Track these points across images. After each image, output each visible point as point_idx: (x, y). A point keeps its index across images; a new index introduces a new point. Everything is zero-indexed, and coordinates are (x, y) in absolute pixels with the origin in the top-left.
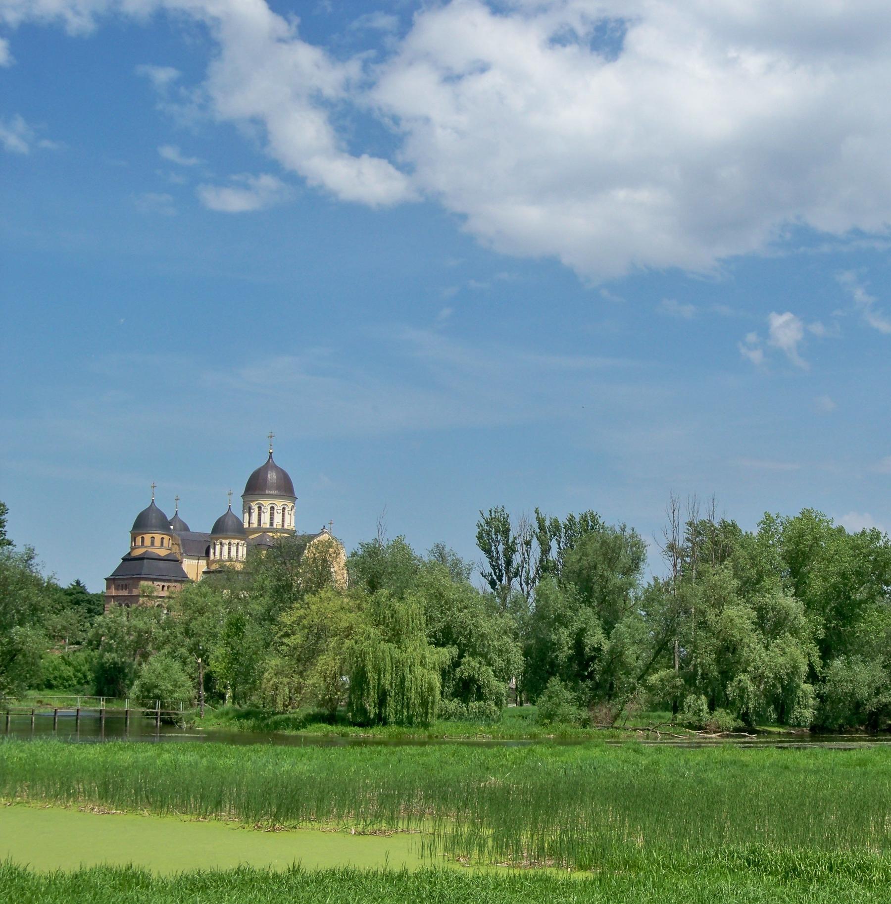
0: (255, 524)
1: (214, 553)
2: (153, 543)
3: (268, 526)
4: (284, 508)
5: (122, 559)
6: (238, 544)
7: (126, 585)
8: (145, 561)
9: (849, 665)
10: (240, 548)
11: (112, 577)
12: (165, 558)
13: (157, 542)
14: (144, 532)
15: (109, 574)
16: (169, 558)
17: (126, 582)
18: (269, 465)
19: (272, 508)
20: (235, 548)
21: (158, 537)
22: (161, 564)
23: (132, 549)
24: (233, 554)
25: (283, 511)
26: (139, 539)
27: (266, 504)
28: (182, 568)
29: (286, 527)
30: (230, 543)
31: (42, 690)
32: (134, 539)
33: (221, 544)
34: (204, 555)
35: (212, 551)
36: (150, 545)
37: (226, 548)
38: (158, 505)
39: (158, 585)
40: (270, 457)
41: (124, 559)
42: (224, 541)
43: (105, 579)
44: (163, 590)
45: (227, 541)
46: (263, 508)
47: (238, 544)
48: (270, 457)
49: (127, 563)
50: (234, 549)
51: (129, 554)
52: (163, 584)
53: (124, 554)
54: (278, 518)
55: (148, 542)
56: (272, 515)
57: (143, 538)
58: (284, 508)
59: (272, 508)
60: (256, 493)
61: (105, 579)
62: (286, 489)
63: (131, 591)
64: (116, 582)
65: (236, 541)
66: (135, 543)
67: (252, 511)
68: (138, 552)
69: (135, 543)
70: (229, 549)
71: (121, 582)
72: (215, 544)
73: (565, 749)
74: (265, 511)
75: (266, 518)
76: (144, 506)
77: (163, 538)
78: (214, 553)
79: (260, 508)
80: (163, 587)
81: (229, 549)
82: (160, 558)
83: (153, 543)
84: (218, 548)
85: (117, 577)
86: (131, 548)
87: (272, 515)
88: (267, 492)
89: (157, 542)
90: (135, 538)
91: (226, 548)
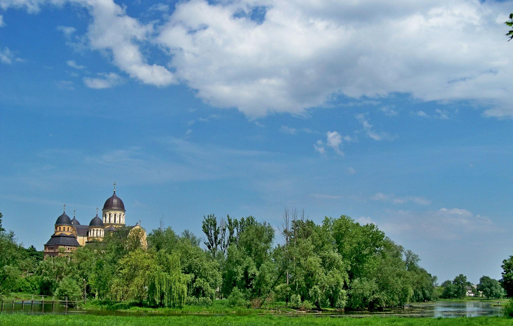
1: (91, 234)
2: (64, 230)
4: (120, 215)
6: (101, 230)
7: (53, 248)
13: (66, 229)
14: (61, 225)
15: (45, 243)
17: (53, 246)
18: (114, 196)
19: (115, 215)
20: (99, 232)
21: (66, 227)
23: (56, 232)
24: (99, 234)
25: (120, 216)
26: (58, 228)
27: (113, 213)
29: (121, 223)
30: (97, 230)
32: (56, 228)
33: (93, 230)
35: (89, 233)
36: (63, 230)
37: (95, 232)
40: (114, 193)
41: (52, 237)
42: (94, 229)
44: (68, 250)
45: (96, 229)
47: (101, 230)
48: (114, 193)
50: (99, 232)
51: (54, 234)
52: (69, 247)
54: (117, 219)
55: (62, 229)
57: (60, 228)
58: (120, 215)
59: (115, 215)
60: (109, 208)
63: (55, 250)
65: (100, 229)
67: (107, 216)
68: (58, 234)
70: (97, 232)
71: (51, 246)
72: (91, 230)
74: (112, 216)
75: (112, 219)
78: (91, 234)
79: (110, 215)
80: (69, 248)
81: (97, 232)
83: (64, 230)
84: (92, 232)
88: (113, 208)
89: (66, 229)
91: (95, 232)
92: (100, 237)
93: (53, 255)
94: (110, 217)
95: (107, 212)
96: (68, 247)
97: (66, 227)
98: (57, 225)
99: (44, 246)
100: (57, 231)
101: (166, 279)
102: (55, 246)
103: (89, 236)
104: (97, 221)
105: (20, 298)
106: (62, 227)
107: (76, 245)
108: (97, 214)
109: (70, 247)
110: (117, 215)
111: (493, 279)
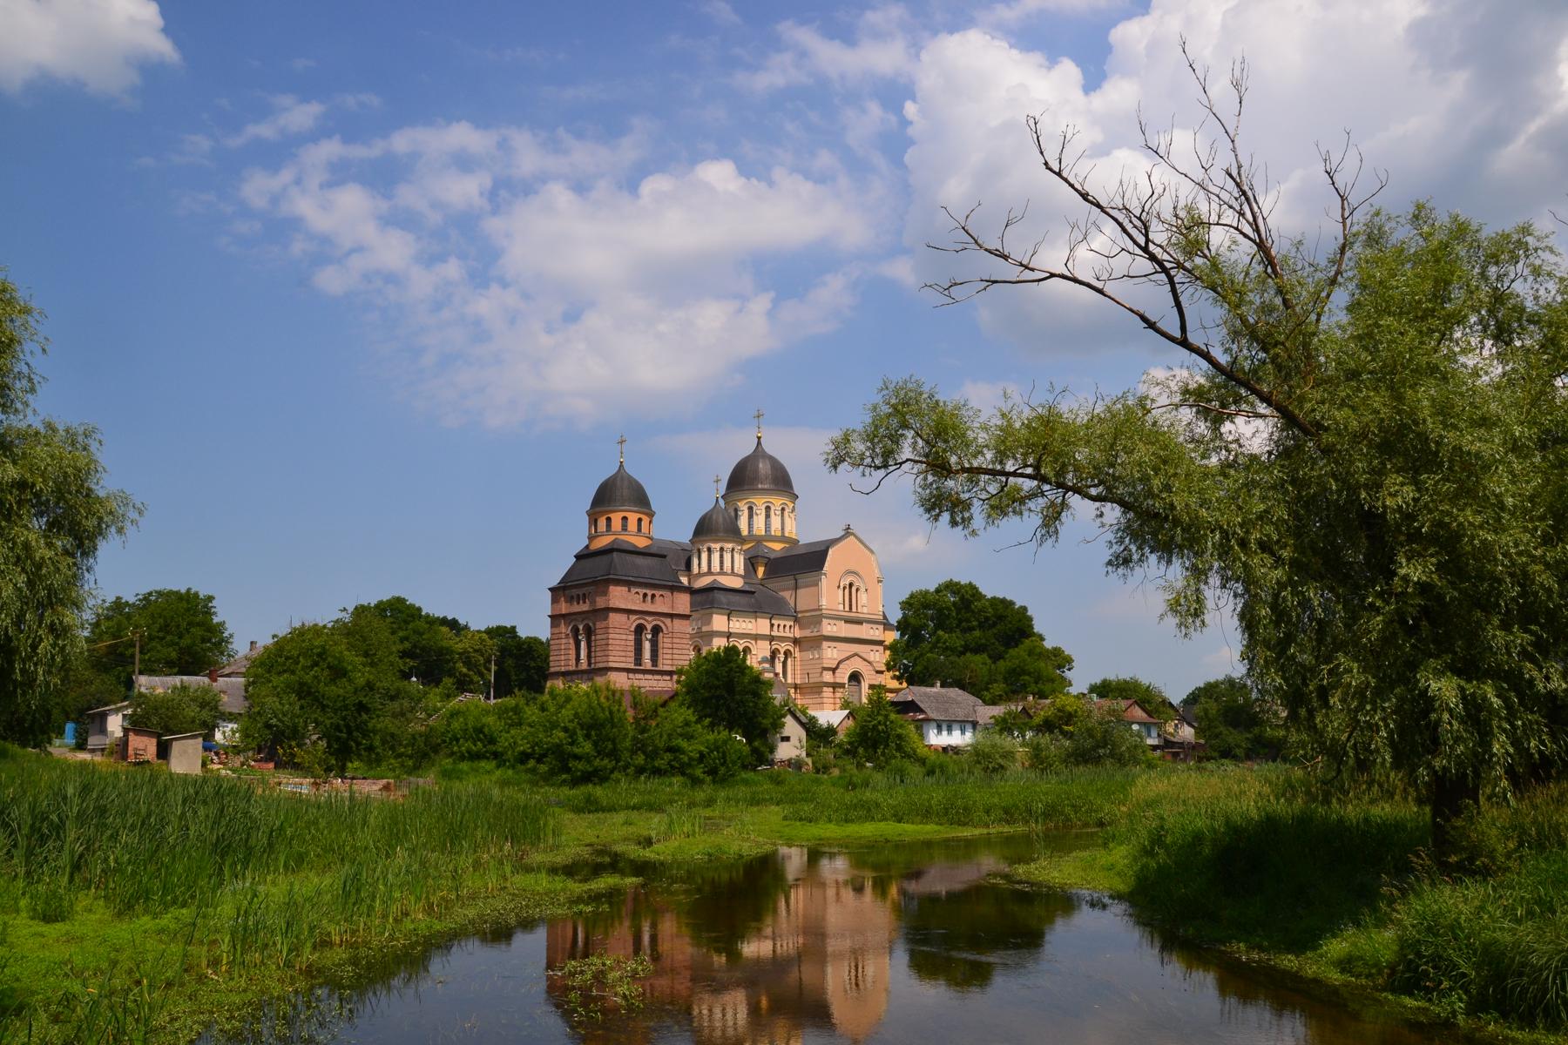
0: (705, 568)
1: (699, 564)
2: (625, 528)
4: (783, 509)
6: (733, 550)
7: (584, 595)
8: (615, 554)
10: (736, 556)
12: (647, 551)
13: (632, 526)
14: (611, 508)
15: (555, 582)
17: (584, 590)
18: (759, 454)
19: (768, 508)
20: (729, 555)
21: (633, 518)
22: (640, 560)
23: (591, 538)
24: (727, 563)
25: (782, 513)
26: (602, 523)
27: (760, 502)
28: (1078, 66)
29: (787, 535)
30: (722, 549)
31: (696, 782)
32: (594, 522)
33: (709, 550)
34: (683, 568)
35: (695, 561)
36: (620, 529)
37: (716, 557)
39: (637, 593)
40: (759, 443)
41: (579, 557)
42: (713, 546)
44: (644, 601)
45: (718, 546)
46: (755, 508)
47: (733, 550)
48: (759, 443)
49: (587, 563)
50: (727, 557)
51: (587, 547)
52: (644, 591)
53: (580, 543)
54: (776, 522)
57: (609, 520)
58: (783, 509)
59: (768, 508)
60: (746, 487)
63: (593, 602)
64: (567, 592)
65: (730, 546)
66: (596, 529)
67: (740, 513)
68: (603, 542)
69: (596, 529)
70: (721, 556)
71: (575, 592)
72: (699, 552)
74: (758, 512)
75: (759, 522)
76: (610, 471)
77: (640, 520)
78: (699, 564)
79: (750, 509)
80: (645, 595)
81: (721, 556)
83: (625, 528)
84: (704, 556)
86: (589, 538)
88: (760, 486)
89: (632, 526)
90: (596, 521)
91: (716, 557)
92: (733, 573)
93: (585, 622)
94: (751, 516)
95: (740, 500)
96: (642, 591)
97: (633, 518)
98: (598, 509)
99: (550, 593)
100: (596, 531)
101: (156, 851)
102: (591, 588)
103: (695, 570)
104: (763, 467)
105: (139, 768)
106: (616, 519)
107: (670, 584)
108: (759, 438)
109: (650, 593)
110: (773, 508)
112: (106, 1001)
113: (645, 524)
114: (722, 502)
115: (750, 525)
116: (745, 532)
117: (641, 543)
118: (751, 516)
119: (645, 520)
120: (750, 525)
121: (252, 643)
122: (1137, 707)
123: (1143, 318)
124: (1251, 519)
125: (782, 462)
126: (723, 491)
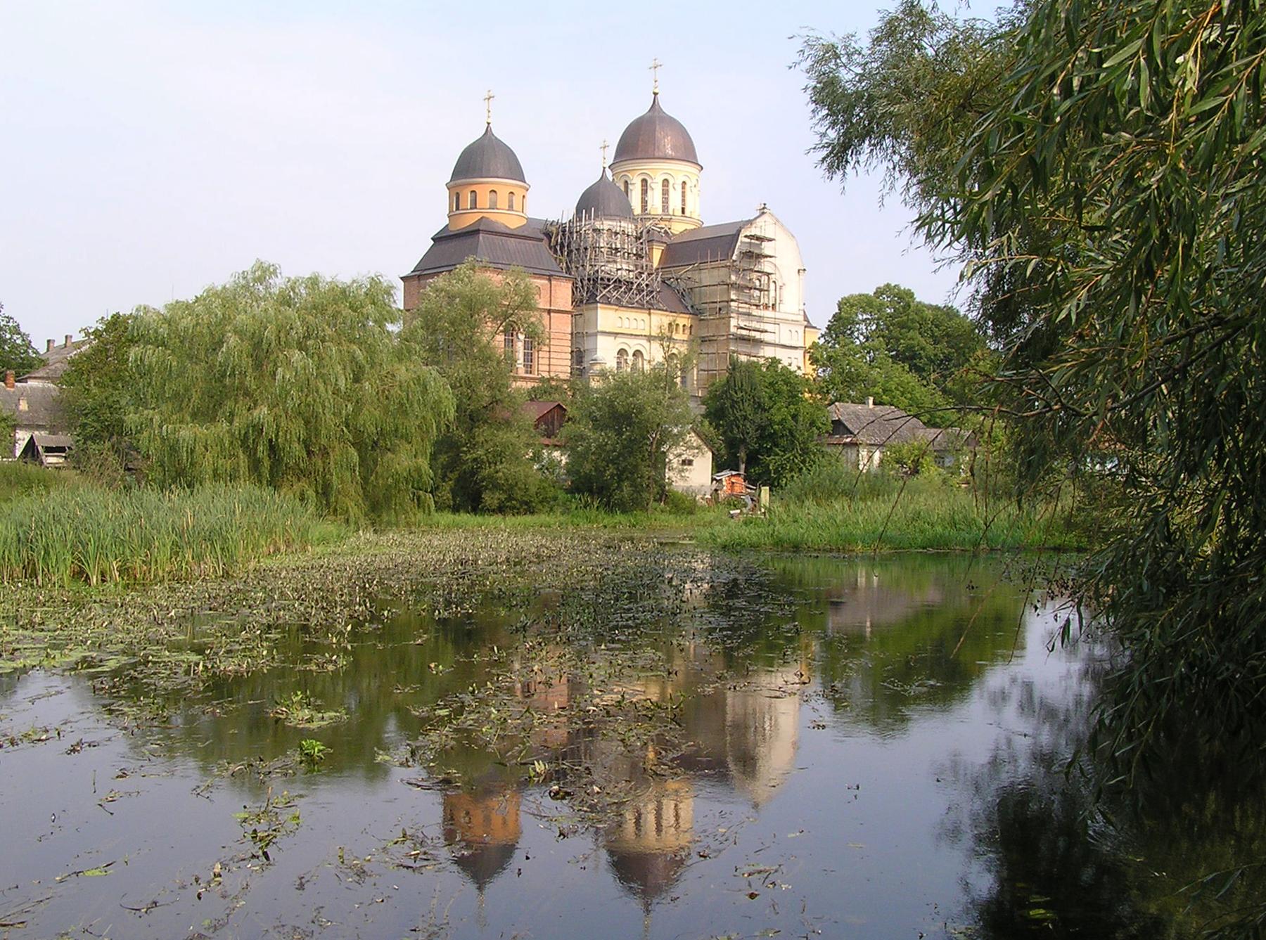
3: (660, 212)
5: (432, 239)
9: (1031, 703)
11: (413, 274)
13: (502, 200)
15: (407, 271)
16: (525, 234)
25: (683, 188)
32: (456, 199)
38: (498, 133)
43: (402, 278)
46: (649, 181)
49: (446, 246)
55: (484, 199)
56: (665, 193)
61: (402, 278)
62: (220, 876)
67: (630, 187)
68: (469, 220)
73: (1185, 58)
82: (508, 232)
85: (425, 272)
87: (665, 193)
94: (644, 192)
98: (459, 181)
100: (457, 208)
111: (931, 305)
112: (987, 253)
113: (517, 200)
114: (609, 174)
115: (644, 203)
116: (637, 210)
117: (513, 222)
118: (644, 192)
119: (519, 193)
120: (644, 203)
121: (49, 341)
122: (570, 285)
123: (387, 801)
124: (864, 312)
125: (695, 145)
126: (610, 161)
